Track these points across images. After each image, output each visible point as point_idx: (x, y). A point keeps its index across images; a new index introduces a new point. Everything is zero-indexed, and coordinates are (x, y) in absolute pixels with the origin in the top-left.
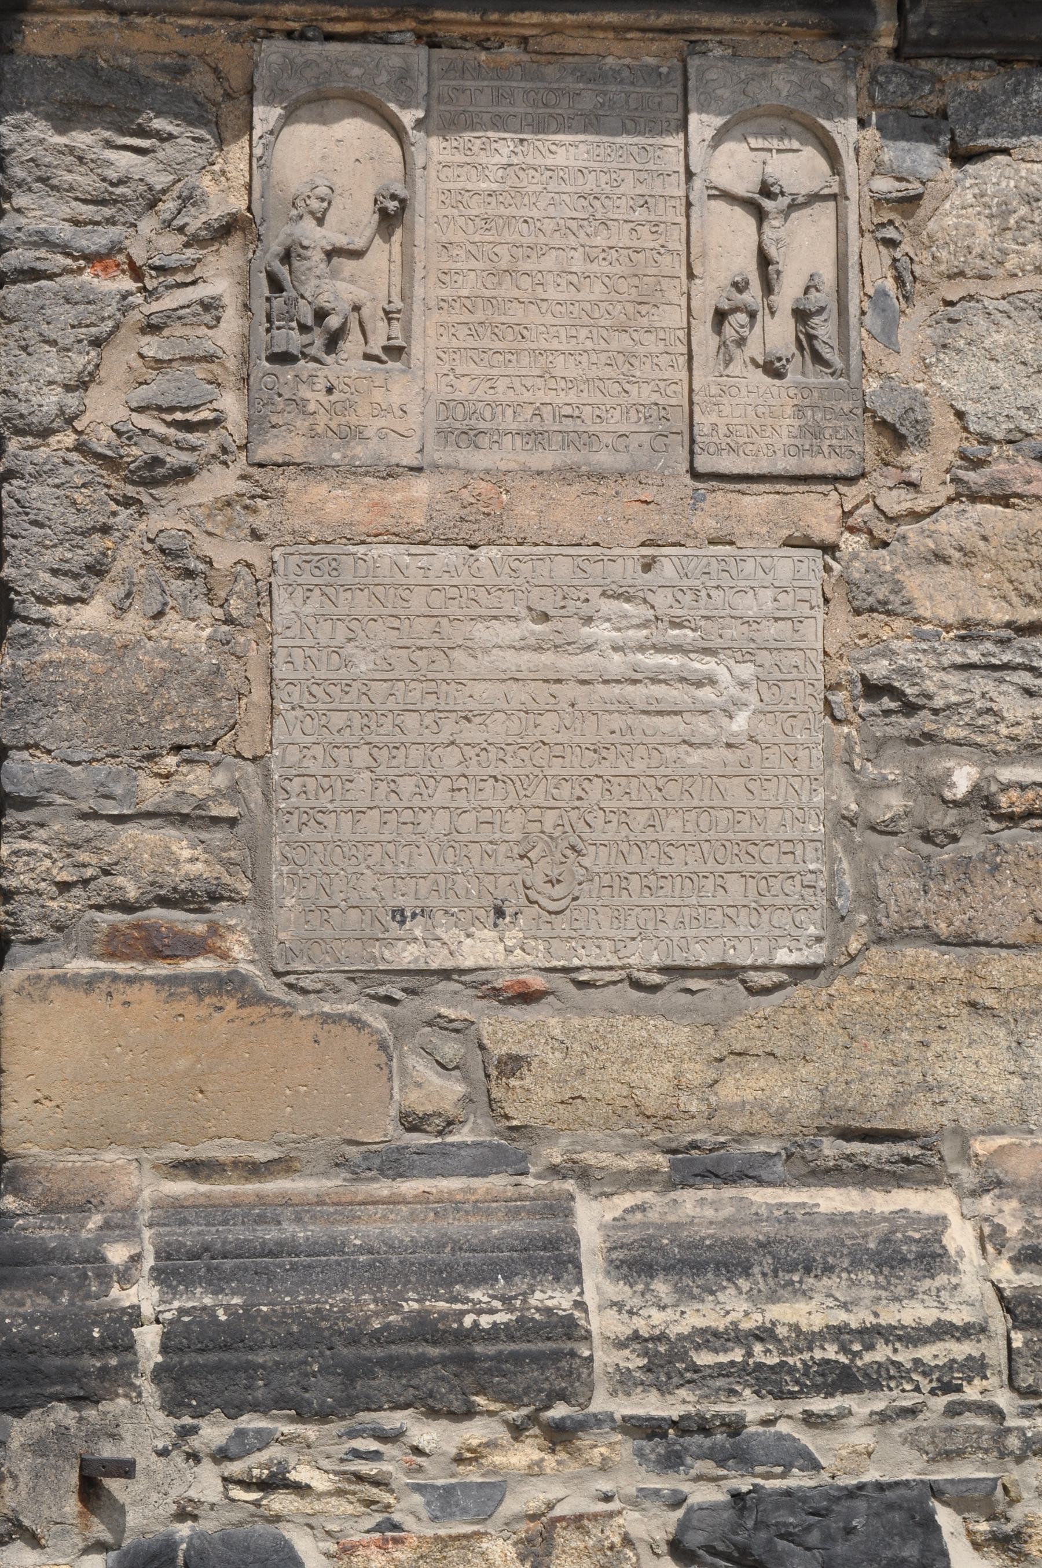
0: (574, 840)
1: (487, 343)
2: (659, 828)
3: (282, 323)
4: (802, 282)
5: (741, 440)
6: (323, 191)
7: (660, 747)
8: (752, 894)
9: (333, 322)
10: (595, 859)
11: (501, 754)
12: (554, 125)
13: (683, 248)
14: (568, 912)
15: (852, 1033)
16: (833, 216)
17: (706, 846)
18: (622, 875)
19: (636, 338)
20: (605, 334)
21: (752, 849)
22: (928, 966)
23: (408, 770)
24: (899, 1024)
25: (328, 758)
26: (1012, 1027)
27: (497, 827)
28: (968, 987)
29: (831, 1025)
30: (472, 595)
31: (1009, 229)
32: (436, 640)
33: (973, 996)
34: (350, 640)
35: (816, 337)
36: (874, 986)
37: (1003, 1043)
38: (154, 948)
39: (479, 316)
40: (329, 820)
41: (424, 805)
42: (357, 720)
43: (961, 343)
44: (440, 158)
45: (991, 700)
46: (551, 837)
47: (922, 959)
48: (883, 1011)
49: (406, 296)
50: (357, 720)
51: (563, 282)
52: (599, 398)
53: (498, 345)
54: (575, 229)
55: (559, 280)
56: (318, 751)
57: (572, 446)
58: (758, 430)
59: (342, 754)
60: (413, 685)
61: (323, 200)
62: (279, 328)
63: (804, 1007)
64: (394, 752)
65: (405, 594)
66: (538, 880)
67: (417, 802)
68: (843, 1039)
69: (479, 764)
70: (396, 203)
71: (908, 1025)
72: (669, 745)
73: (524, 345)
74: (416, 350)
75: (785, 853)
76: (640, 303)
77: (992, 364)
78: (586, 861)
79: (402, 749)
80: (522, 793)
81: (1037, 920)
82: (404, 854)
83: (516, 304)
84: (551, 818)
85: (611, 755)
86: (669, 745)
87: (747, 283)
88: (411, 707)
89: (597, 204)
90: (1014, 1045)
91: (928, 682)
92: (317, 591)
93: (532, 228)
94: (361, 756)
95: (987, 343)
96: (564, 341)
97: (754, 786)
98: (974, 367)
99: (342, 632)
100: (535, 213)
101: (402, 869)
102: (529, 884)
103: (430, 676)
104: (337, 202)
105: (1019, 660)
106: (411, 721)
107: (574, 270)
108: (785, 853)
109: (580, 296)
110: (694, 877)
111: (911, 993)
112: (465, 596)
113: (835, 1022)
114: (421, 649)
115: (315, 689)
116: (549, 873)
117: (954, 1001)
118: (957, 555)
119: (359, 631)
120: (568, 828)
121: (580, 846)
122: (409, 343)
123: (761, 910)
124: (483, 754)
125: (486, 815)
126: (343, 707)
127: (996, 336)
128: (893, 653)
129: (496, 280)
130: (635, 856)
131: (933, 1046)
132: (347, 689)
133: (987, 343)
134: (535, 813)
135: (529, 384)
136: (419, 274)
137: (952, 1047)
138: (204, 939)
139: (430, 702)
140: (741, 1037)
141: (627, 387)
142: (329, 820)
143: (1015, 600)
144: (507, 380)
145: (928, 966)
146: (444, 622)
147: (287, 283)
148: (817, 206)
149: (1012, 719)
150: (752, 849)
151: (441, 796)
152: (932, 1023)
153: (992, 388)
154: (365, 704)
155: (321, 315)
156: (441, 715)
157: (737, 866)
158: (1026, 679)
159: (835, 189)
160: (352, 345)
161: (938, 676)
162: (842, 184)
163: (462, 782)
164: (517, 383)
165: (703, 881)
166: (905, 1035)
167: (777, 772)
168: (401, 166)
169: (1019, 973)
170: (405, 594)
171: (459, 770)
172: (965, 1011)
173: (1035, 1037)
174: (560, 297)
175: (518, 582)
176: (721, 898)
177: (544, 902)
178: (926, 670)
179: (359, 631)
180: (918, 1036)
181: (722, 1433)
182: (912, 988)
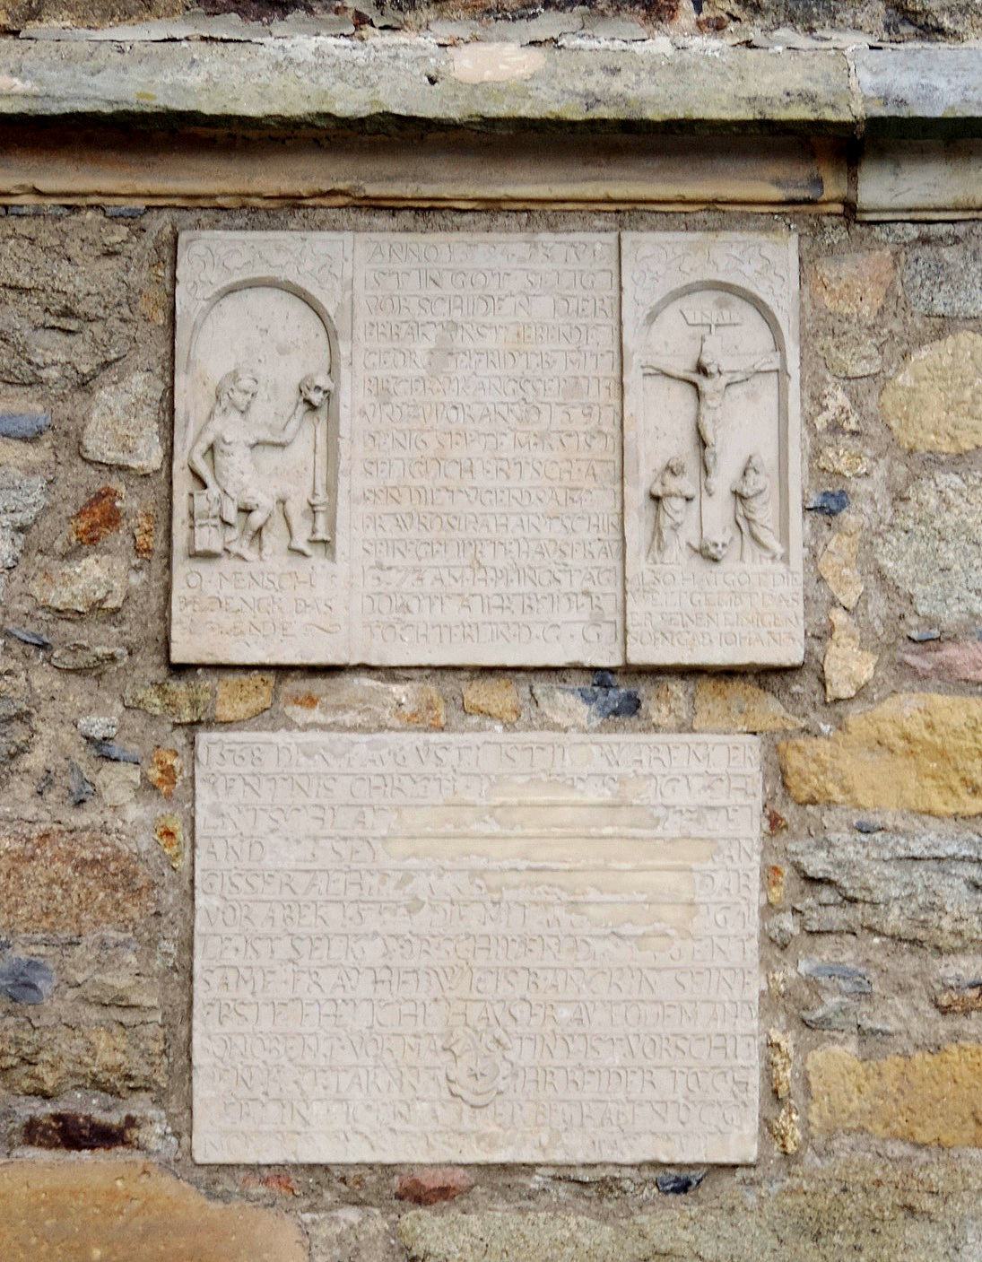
0: (499, 1033)
1: (412, 533)
2: (585, 1021)
3: (204, 522)
4: (739, 464)
5: (676, 629)
6: (246, 383)
7: (588, 940)
8: (681, 1090)
9: (257, 518)
10: (523, 1054)
11: (425, 946)
12: (537, 124)
13: (615, 431)
14: (491, 1107)
15: (782, 1236)
16: (776, 392)
17: (633, 1041)
18: (548, 1069)
19: (569, 525)
20: (536, 521)
21: (681, 1043)
22: (862, 1169)
23: (331, 962)
24: (831, 1227)
25: (249, 948)
26: (950, 1232)
27: (420, 1020)
28: (904, 1190)
29: (760, 1227)
30: (396, 783)
31: (964, 402)
32: (359, 831)
33: (910, 1199)
34: (272, 831)
35: (754, 521)
36: (805, 1188)
37: (940, 1249)
38: (70, 1138)
39: (406, 506)
40: (250, 1012)
41: (347, 997)
42: (279, 913)
43: (910, 524)
44: (367, 345)
45: (935, 893)
46: (476, 1032)
47: (856, 1160)
48: (814, 1214)
49: (331, 489)
50: (279, 913)
51: (492, 468)
52: (527, 587)
53: (427, 536)
54: (505, 414)
55: (489, 467)
56: (240, 942)
57: (501, 638)
58: (694, 618)
59: (262, 946)
60: (335, 876)
61: (246, 392)
62: (201, 526)
63: (733, 1208)
64: (317, 944)
65: (330, 784)
66: (458, 1072)
67: (339, 994)
68: (774, 1243)
69: (403, 956)
70: (321, 394)
71: (841, 1228)
72: (598, 937)
73: (455, 534)
74: (341, 543)
75: (716, 1048)
76: (572, 489)
77: (943, 545)
78: (511, 1056)
79: (325, 941)
80: (446, 985)
81: (977, 1121)
82: (324, 1048)
83: (444, 493)
84: (475, 1011)
85: (536, 947)
86: (598, 937)
87: (683, 467)
88: (334, 898)
89: (528, 387)
90: (951, 1251)
91: (868, 875)
92: (239, 783)
93: (461, 415)
94: (283, 950)
95: (938, 523)
96: (494, 529)
97: (686, 979)
98: (923, 547)
99: (264, 823)
100: (466, 401)
101: (322, 1062)
102: (452, 1078)
103: (354, 866)
104: (263, 394)
105: (965, 852)
106: (334, 912)
107: (504, 455)
108: (716, 1048)
109: (509, 484)
110: (622, 1073)
111: (843, 1197)
112: (390, 785)
113: (764, 1224)
114: (345, 839)
115: (237, 880)
116: (473, 1066)
117: (889, 1204)
118: (902, 743)
119: (282, 821)
120: (492, 1021)
121: (505, 1040)
122: (334, 537)
123: (690, 1106)
124: (407, 946)
125: (408, 1008)
126: (264, 897)
127: (947, 516)
128: (831, 845)
129: (423, 468)
130: (559, 1052)
131: (866, 1251)
132: (270, 880)
133: (938, 523)
134: (461, 1006)
135: (457, 575)
136: (343, 464)
137: (886, 1252)
138: (121, 1131)
139: (353, 893)
140: (666, 1238)
141: (558, 575)
142: (250, 1012)
143: (961, 790)
144: (435, 572)
145: (862, 1169)
146: (369, 813)
147: (209, 479)
148: (756, 381)
149: (957, 914)
150: (681, 1043)
151: (364, 988)
152: (866, 1225)
153: (942, 570)
154: (287, 894)
155: (246, 511)
156: (366, 906)
157: (666, 1060)
158: (973, 872)
159: (776, 365)
160: (274, 540)
161: (877, 868)
162: (784, 359)
163: (384, 975)
164: (445, 573)
165: (631, 1077)
166: (836, 1239)
167: (708, 964)
168: (327, 354)
169: (958, 1177)
170: (330, 784)
171: (382, 962)
172: (901, 1215)
173: (973, 1244)
174: (490, 485)
175: (444, 770)
176: (649, 1093)
177: (466, 1095)
178: (866, 863)
179: (282, 821)
180: (851, 1240)
181: (49, 591)
182: (845, 1190)
